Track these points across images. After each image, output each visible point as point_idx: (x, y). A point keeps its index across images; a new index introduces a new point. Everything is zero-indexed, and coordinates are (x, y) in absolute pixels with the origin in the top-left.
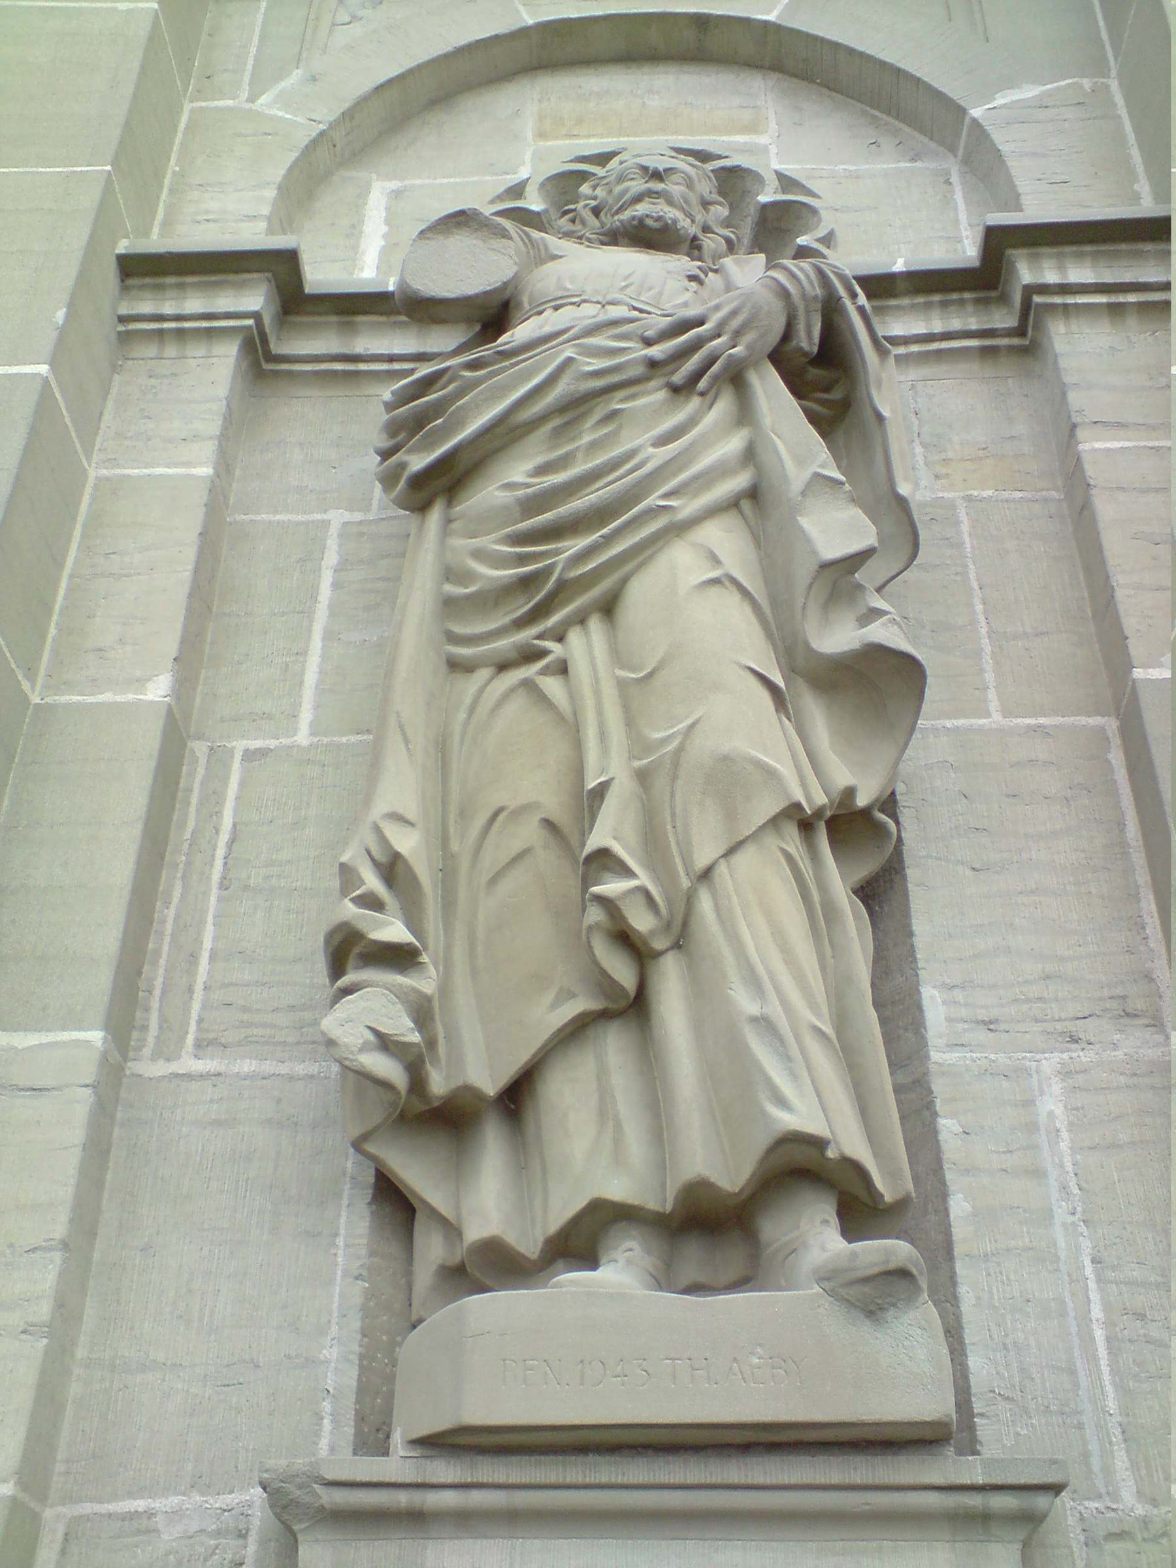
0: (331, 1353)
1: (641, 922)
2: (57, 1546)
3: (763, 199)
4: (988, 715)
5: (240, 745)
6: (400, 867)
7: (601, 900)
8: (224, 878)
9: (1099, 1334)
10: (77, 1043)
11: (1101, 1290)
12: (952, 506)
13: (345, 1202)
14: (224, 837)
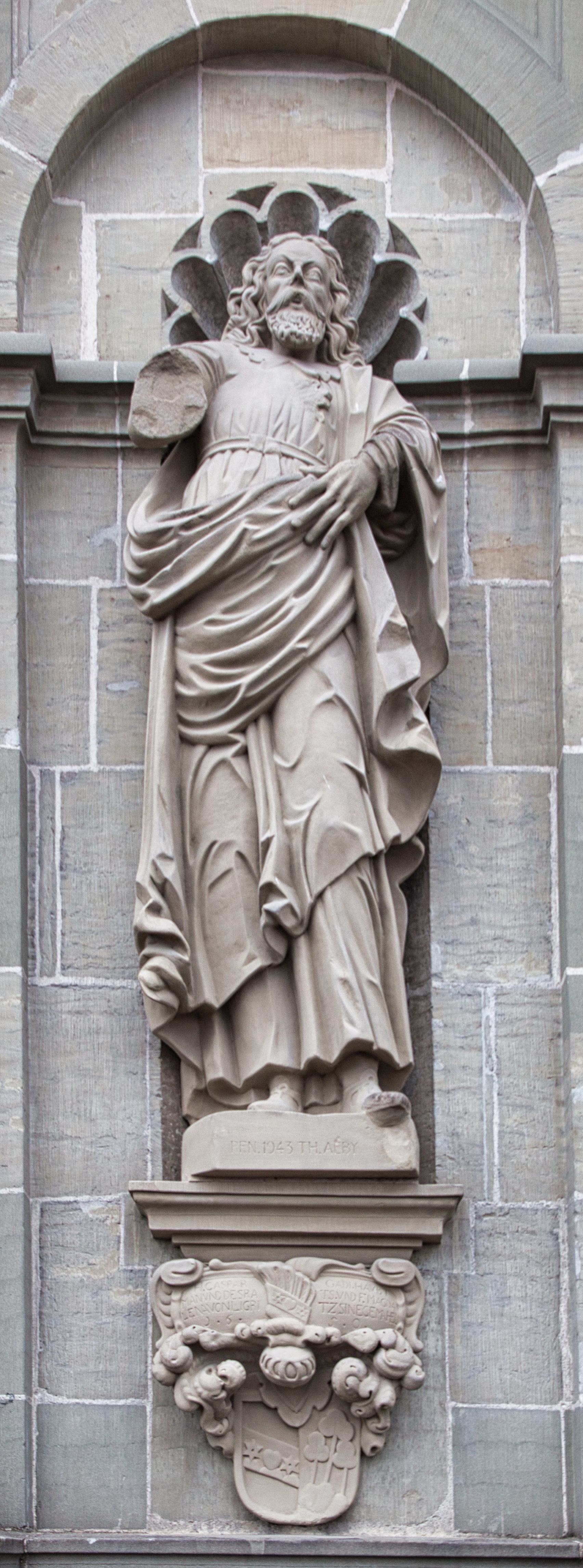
0: (148, 1132)
1: (289, 922)
2: (38, 1214)
3: (378, 258)
4: (485, 763)
5: (58, 769)
6: (168, 887)
7: (269, 913)
8: (61, 863)
9: (496, 1129)
10: (9, 973)
11: (500, 1108)
12: (482, 587)
13: (148, 1056)
14: (58, 836)
